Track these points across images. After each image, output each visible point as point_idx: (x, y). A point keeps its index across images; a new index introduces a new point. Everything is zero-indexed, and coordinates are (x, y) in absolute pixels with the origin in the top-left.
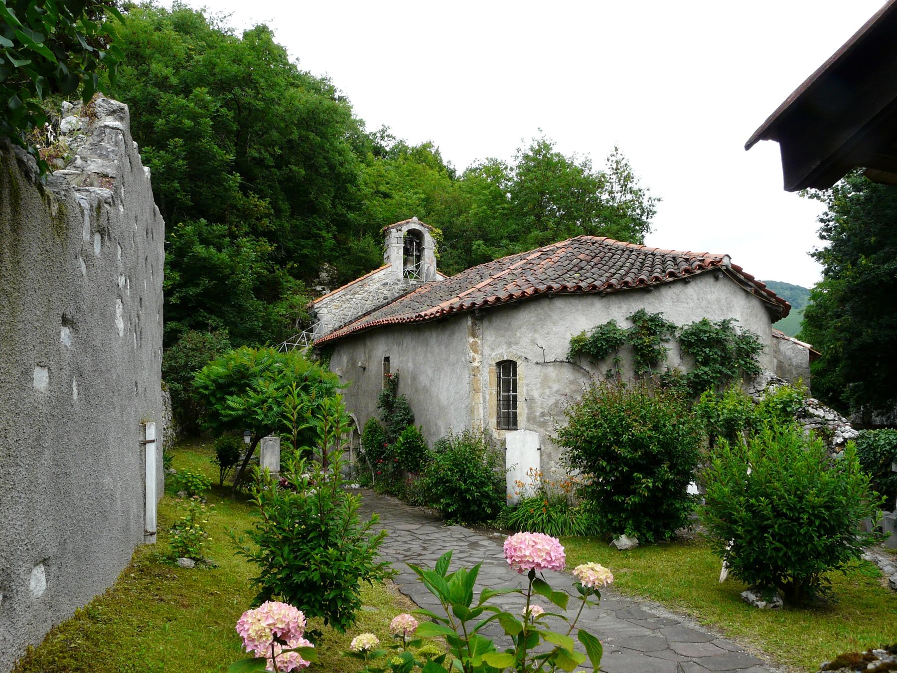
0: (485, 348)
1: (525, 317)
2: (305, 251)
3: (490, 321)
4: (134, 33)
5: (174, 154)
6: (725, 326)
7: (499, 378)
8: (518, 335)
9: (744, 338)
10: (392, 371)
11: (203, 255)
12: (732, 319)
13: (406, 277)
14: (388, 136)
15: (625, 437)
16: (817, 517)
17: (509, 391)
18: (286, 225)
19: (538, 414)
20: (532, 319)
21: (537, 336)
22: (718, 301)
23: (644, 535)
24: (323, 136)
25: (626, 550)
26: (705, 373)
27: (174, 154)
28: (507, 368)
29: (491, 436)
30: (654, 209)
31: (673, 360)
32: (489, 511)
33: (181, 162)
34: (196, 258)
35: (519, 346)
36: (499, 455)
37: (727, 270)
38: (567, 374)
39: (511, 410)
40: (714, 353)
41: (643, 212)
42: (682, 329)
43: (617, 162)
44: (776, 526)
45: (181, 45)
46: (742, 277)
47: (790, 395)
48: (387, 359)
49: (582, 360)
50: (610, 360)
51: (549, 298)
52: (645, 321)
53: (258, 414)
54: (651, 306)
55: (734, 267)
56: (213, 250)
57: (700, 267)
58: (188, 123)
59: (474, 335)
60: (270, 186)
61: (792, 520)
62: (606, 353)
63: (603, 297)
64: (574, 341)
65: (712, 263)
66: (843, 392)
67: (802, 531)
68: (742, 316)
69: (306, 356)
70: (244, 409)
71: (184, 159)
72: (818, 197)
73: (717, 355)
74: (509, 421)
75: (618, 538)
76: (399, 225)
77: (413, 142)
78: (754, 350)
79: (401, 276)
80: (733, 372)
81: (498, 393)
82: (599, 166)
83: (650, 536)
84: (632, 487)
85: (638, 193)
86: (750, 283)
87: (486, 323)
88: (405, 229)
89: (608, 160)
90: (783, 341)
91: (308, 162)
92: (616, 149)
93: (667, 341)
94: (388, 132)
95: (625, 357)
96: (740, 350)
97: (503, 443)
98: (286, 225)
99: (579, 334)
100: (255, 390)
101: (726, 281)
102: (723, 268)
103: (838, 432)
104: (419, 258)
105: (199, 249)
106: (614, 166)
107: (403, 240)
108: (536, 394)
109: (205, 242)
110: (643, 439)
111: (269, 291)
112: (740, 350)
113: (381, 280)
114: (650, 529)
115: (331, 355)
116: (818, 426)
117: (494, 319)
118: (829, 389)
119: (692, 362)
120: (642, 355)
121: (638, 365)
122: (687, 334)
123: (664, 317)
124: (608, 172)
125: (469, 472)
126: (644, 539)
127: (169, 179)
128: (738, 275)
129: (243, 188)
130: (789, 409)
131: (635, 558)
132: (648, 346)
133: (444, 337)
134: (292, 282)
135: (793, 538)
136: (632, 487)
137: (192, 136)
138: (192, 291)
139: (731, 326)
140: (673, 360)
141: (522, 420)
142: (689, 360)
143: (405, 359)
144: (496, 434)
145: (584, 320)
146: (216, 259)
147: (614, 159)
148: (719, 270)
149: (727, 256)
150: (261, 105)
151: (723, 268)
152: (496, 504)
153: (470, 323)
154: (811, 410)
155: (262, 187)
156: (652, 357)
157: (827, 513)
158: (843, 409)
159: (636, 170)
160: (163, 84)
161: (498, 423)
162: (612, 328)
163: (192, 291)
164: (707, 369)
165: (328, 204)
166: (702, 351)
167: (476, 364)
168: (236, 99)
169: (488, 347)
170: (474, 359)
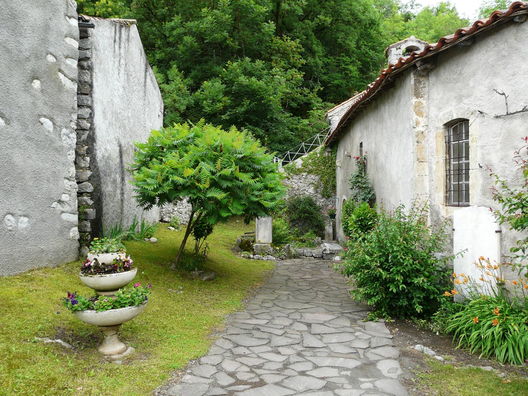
0: (432, 109)
2: (336, 82)
3: (437, 76)
7: (448, 143)
8: (471, 84)
10: (364, 154)
11: (245, 83)
14: (416, 5)
17: (459, 158)
28: (458, 127)
29: (438, 213)
32: (419, 309)
33: (227, 16)
34: (241, 85)
35: (473, 98)
36: (443, 236)
39: (463, 182)
48: (361, 144)
51: (515, 23)
59: (417, 95)
69: (320, 153)
76: (398, 44)
81: (448, 162)
87: (432, 79)
105: (243, 79)
108: (494, 159)
109: (249, 74)
111: (302, 110)
129: (278, 33)
141: (475, 193)
144: (444, 212)
152: (435, 298)
153: (412, 82)
161: (447, 199)
167: (420, 129)
170: (417, 123)
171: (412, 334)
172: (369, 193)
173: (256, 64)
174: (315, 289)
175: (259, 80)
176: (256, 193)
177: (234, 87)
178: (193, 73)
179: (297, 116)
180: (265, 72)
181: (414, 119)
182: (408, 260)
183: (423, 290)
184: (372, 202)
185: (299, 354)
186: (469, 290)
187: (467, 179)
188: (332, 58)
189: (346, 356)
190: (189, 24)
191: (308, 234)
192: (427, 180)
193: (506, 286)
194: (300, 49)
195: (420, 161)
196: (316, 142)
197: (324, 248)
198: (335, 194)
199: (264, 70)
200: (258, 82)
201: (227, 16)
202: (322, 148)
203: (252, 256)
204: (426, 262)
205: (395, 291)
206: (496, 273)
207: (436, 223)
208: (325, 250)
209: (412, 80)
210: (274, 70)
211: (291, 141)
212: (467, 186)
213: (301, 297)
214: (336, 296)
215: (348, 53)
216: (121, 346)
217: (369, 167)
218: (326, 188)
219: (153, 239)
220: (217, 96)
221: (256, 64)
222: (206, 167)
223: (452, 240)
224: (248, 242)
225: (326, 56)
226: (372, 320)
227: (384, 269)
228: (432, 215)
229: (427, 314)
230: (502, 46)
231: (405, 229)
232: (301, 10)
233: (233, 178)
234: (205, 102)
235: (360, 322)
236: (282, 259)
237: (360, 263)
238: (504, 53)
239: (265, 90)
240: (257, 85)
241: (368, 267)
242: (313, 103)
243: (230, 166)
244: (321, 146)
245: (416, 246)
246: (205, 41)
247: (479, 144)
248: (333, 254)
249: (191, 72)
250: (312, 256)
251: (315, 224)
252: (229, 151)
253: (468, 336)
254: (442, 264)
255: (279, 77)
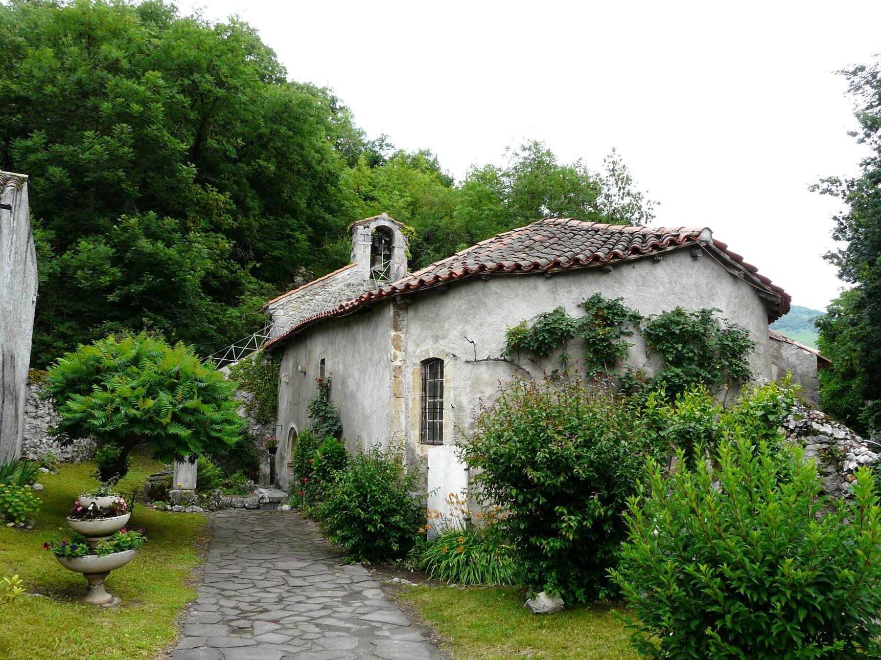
0: (410, 343)
1: (455, 304)
2: (276, 253)
3: (416, 310)
4: (84, 13)
5: (120, 140)
6: (705, 317)
7: (424, 380)
8: (447, 327)
9: (730, 334)
10: (327, 375)
11: (148, 250)
12: (714, 309)
13: (371, 277)
14: (387, 145)
15: (540, 456)
16: (801, 604)
17: (435, 397)
18: (254, 223)
19: (467, 425)
20: (463, 307)
21: (468, 328)
22: (697, 286)
23: (573, 594)
24: (297, 132)
25: (546, 614)
26: (677, 375)
27: (120, 140)
29: (413, 451)
30: (652, 213)
31: (636, 356)
33: (126, 149)
34: (140, 252)
36: (418, 475)
37: (708, 246)
38: (503, 374)
40: (692, 351)
41: (642, 216)
42: (649, 319)
43: (614, 163)
44: (728, 617)
45: (140, 33)
46: (728, 257)
47: (773, 397)
48: (323, 361)
49: (521, 357)
50: (556, 356)
52: (599, 309)
53: (94, 417)
54: (607, 289)
55: (716, 243)
56: (160, 245)
57: (672, 242)
58: (136, 107)
59: (396, 328)
60: (235, 182)
61: (757, 607)
62: (550, 349)
63: (548, 278)
64: (512, 334)
65: (688, 238)
66: (861, 412)
67: (775, 630)
68: (728, 308)
69: (256, 361)
70: (84, 412)
71: (130, 147)
72: (830, 192)
73: (693, 352)
74: (432, 433)
75: (534, 597)
77: (411, 149)
78: (742, 349)
79: (367, 276)
80: (715, 376)
81: (423, 399)
82: (595, 168)
83: (580, 593)
84: (553, 526)
85: (637, 197)
86: (738, 266)
87: (411, 313)
88: (373, 226)
89: (605, 161)
90: (786, 345)
91: (282, 157)
92: (614, 150)
93: (629, 334)
94: (388, 141)
95: (575, 354)
96: (724, 347)
97: (425, 459)
98: (254, 223)
99: (518, 324)
100: (105, 388)
101: (708, 262)
102: (703, 245)
103: (851, 455)
104: (388, 257)
105: (144, 244)
106: (611, 168)
107: (370, 237)
108: (465, 400)
109: (153, 236)
110: (567, 459)
111: (226, 292)
112: (724, 347)
113: (345, 279)
114: (580, 585)
115: (281, 360)
116: (825, 446)
117: (420, 308)
118: (847, 411)
119: (661, 362)
120: (596, 352)
121: (590, 363)
122: (655, 326)
123: (625, 304)
124: (604, 174)
125: (373, 496)
126: (571, 599)
127: (114, 167)
128: (722, 254)
130: (771, 418)
131: (550, 628)
132: (603, 340)
133: (369, 332)
134: (251, 283)
135: (759, 639)
136: (553, 526)
137: (141, 122)
138: (135, 288)
139: (712, 317)
140: (636, 356)
141: (448, 432)
142: (657, 359)
143: (336, 360)
144: (419, 450)
145: (523, 307)
146: (162, 255)
147: (611, 160)
148: (697, 246)
149: (708, 229)
150: (221, 92)
151: (703, 245)
152: (410, 538)
153: (392, 313)
154: (815, 426)
155: (227, 182)
156: (608, 355)
157: (821, 598)
158: (860, 429)
159: (633, 172)
160: (114, 67)
161: (422, 437)
162: (559, 316)
163: (135, 288)
164: (679, 371)
165: (303, 204)
166: (673, 347)
167: (397, 363)
168: (195, 85)
169: (413, 339)
170: (395, 357)
171: (389, 573)
172: (335, 425)
173: (165, 222)
174: (276, 541)
175: (168, 248)
176: (217, 427)
177: (129, 255)
178: (56, 221)
179: (220, 301)
180: (179, 234)
181: (392, 352)
182: (386, 499)
183: (399, 529)
184: (338, 434)
185: (288, 591)
186: (441, 526)
187: (441, 418)
188: (272, 218)
189: (333, 590)
190: (58, 148)
191: (237, 475)
192: (403, 416)
193: (472, 522)
194: (230, 205)
195: (397, 396)
196: (252, 344)
197: (260, 496)
198: (276, 419)
199: (176, 232)
200: (167, 250)
201: (126, 149)
202: (260, 354)
203: (169, 507)
204: (402, 501)
205: (373, 530)
206: (465, 507)
207: (412, 462)
208: (263, 498)
209: (391, 312)
210: (191, 234)
211: (211, 338)
212: (441, 424)
213: (263, 549)
214: (302, 546)
215: (294, 213)
216: (108, 597)
217: (333, 391)
218: (262, 410)
219: (38, 486)
220: (101, 265)
221: (165, 222)
222: (164, 397)
223: (426, 479)
224: (161, 488)
225: (263, 214)
226: (348, 564)
227: (362, 509)
228: (407, 453)
229: (403, 554)
230: (472, 297)
231: (381, 467)
232: (235, 151)
233: (195, 411)
234: (80, 273)
235: (337, 566)
236: (213, 510)
237: (336, 504)
238: (474, 304)
239: (177, 262)
240: (166, 254)
241: (346, 508)
242: (244, 285)
243: (192, 398)
244: (257, 351)
245: (392, 485)
246: (86, 179)
247: (452, 385)
248: (275, 503)
249: (53, 220)
250: (244, 507)
251: (246, 461)
252: (188, 378)
253: (439, 566)
254: (417, 503)
255: (199, 246)
